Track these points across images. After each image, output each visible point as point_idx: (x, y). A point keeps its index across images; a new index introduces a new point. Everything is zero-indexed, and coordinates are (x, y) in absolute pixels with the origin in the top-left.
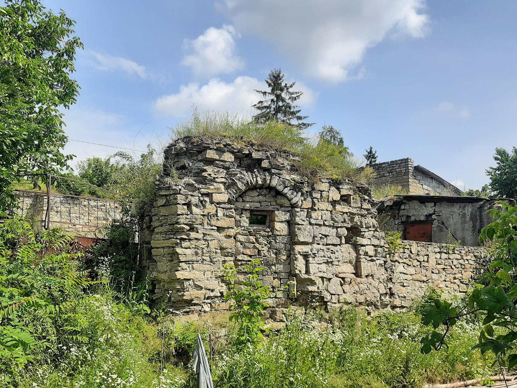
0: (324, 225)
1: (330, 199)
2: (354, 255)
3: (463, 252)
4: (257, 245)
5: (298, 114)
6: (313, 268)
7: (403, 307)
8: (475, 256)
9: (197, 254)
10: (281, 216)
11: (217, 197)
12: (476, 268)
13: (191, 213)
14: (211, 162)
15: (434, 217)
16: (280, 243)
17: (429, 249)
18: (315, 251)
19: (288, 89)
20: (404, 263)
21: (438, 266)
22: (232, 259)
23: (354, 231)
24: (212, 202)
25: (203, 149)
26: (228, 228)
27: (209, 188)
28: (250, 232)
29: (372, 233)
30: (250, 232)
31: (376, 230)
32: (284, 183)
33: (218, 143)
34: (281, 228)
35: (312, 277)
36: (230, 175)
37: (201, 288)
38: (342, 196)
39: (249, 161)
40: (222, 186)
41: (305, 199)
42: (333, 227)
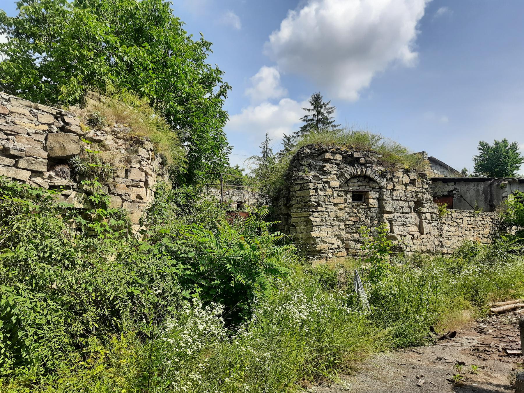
0: (401, 200)
1: (404, 182)
2: (418, 219)
3: (484, 216)
4: (358, 214)
5: (332, 124)
6: (395, 229)
7: (449, 254)
8: (491, 218)
9: (322, 221)
10: (373, 195)
11: (333, 184)
12: (492, 227)
13: (318, 194)
14: (328, 161)
15: (454, 192)
16: (373, 213)
17: (464, 214)
18: (396, 218)
19: (325, 106)
20: (448, 224)
21: (469, 226)
22: (343, 223)
23: (419, 204)
24: (330, 187)
25: (322, 152)
26: (340, 204)
27: (327, 178)
28: (353, 206)
29: (429, 204)
30: (353, 206)
31: (431, 203)
32: (375, 172)
33: (332, 148)
34: (373, 202)
35: (395, 235)
36: (340, 169)
37: (326, 243)
38: (410, 180)
39: (351, 159)
40: (335, 176)
41: (389, 183)
42: (406, 201)
